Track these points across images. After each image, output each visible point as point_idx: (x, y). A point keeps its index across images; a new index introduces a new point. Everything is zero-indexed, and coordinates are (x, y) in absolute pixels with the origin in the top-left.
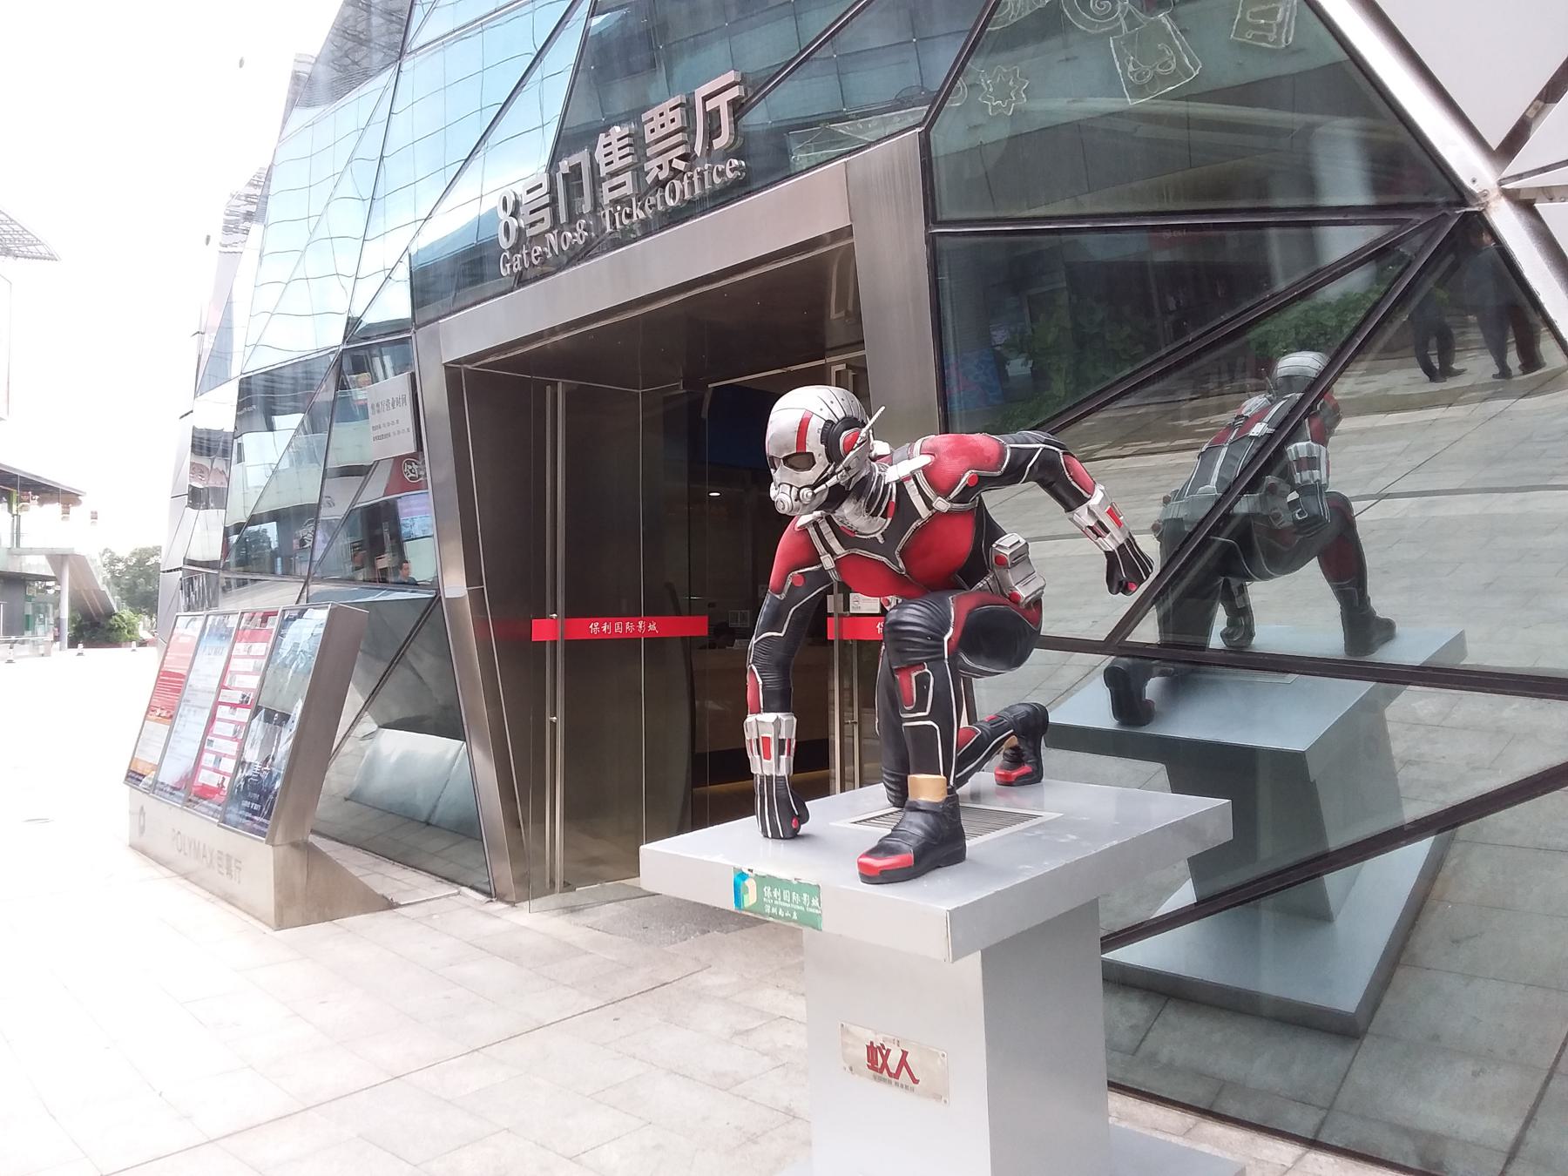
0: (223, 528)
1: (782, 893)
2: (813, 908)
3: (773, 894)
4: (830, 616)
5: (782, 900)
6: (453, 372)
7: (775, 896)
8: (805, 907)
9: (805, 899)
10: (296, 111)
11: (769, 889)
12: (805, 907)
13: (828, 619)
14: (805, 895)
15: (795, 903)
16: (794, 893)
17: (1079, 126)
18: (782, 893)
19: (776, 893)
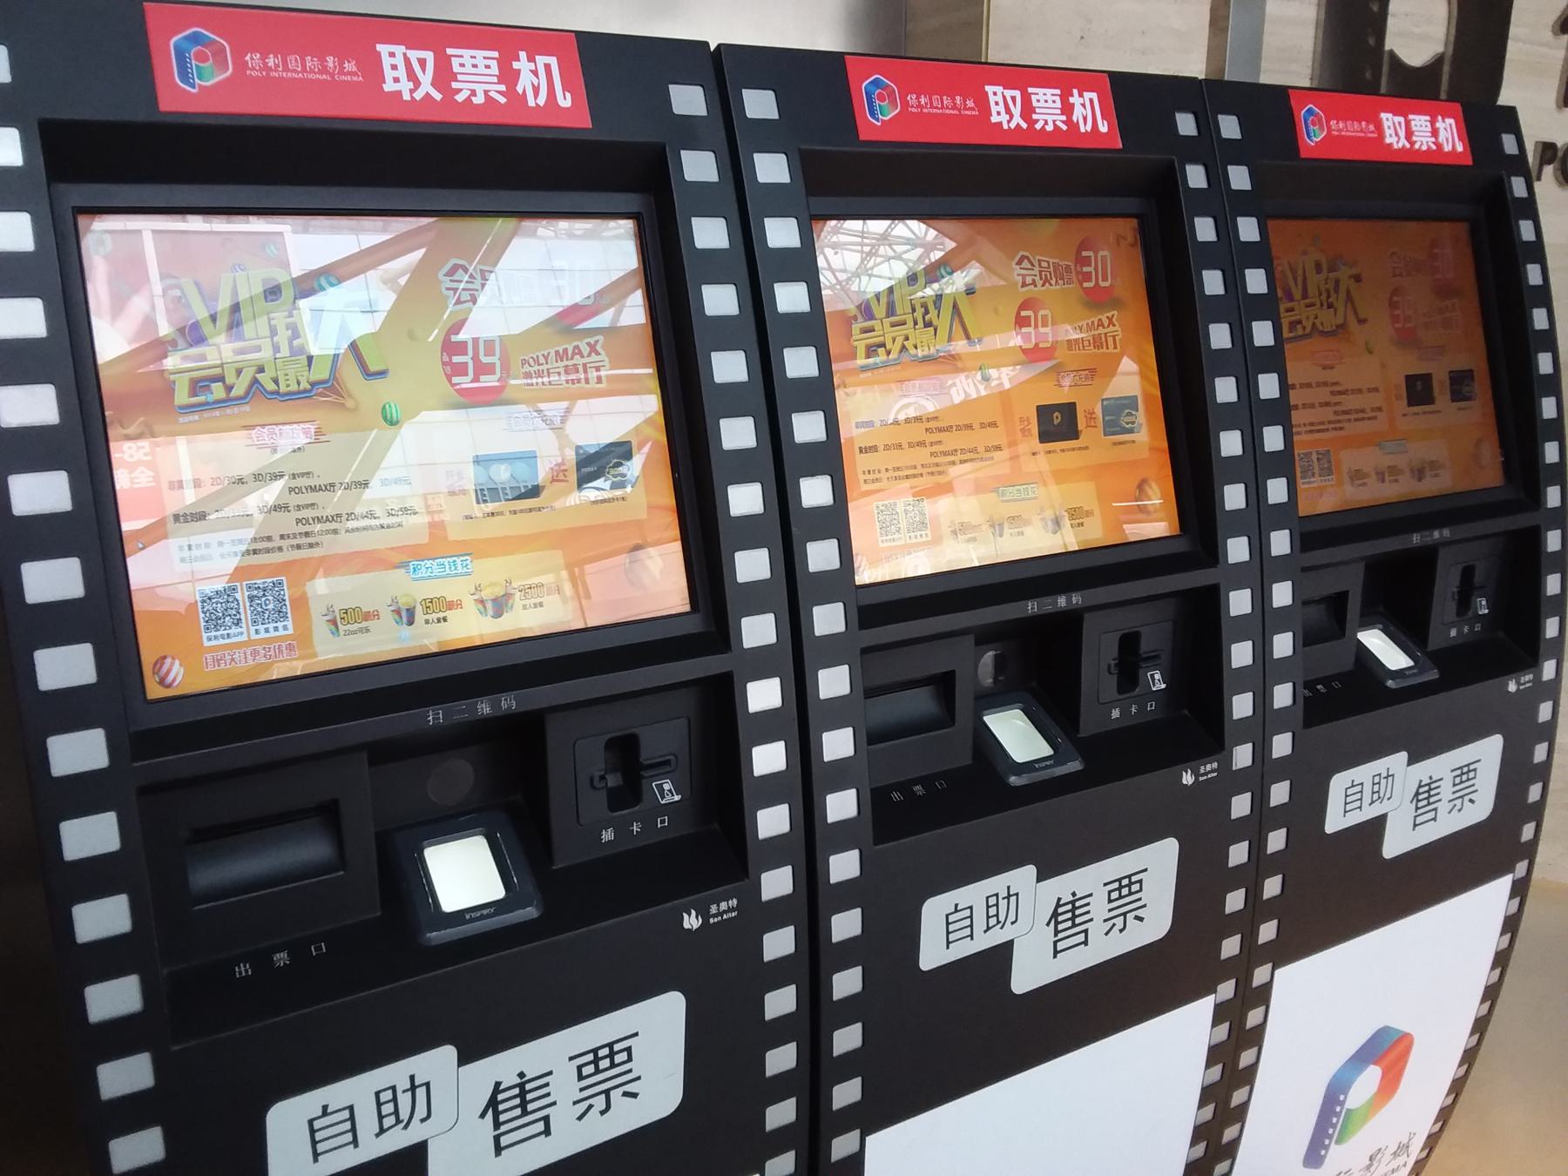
0: (1011, 938)
1: (930, 99)
2: (345, 74)
3: (919, 102)
4: (1292, 389)
5: (932, 107)
6: (467, 355)
7: (923, 103)
8: (332, 75)
9: (958, 102)
10: (1342, 321)
11: (1335, 122)
12: (959, 110)
13: (1290, 391)
14: (958, 98)
15: (947, 108)
16: (945, 97)
17: (491, 272)
18: (930, 99)
19: (271, 61)
